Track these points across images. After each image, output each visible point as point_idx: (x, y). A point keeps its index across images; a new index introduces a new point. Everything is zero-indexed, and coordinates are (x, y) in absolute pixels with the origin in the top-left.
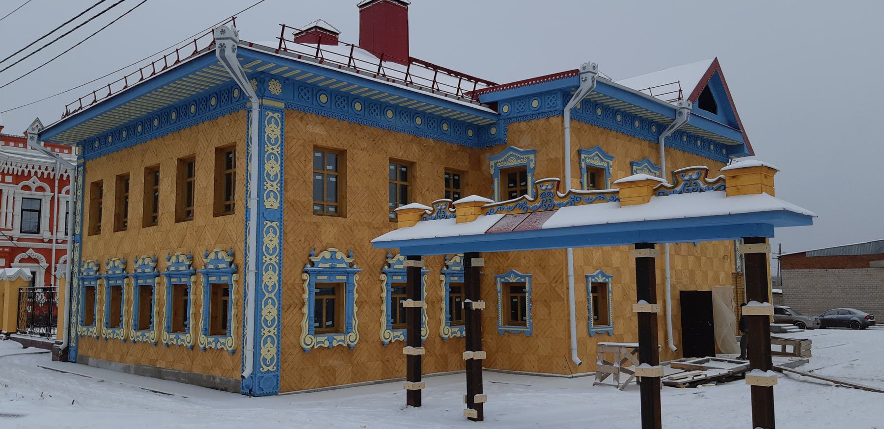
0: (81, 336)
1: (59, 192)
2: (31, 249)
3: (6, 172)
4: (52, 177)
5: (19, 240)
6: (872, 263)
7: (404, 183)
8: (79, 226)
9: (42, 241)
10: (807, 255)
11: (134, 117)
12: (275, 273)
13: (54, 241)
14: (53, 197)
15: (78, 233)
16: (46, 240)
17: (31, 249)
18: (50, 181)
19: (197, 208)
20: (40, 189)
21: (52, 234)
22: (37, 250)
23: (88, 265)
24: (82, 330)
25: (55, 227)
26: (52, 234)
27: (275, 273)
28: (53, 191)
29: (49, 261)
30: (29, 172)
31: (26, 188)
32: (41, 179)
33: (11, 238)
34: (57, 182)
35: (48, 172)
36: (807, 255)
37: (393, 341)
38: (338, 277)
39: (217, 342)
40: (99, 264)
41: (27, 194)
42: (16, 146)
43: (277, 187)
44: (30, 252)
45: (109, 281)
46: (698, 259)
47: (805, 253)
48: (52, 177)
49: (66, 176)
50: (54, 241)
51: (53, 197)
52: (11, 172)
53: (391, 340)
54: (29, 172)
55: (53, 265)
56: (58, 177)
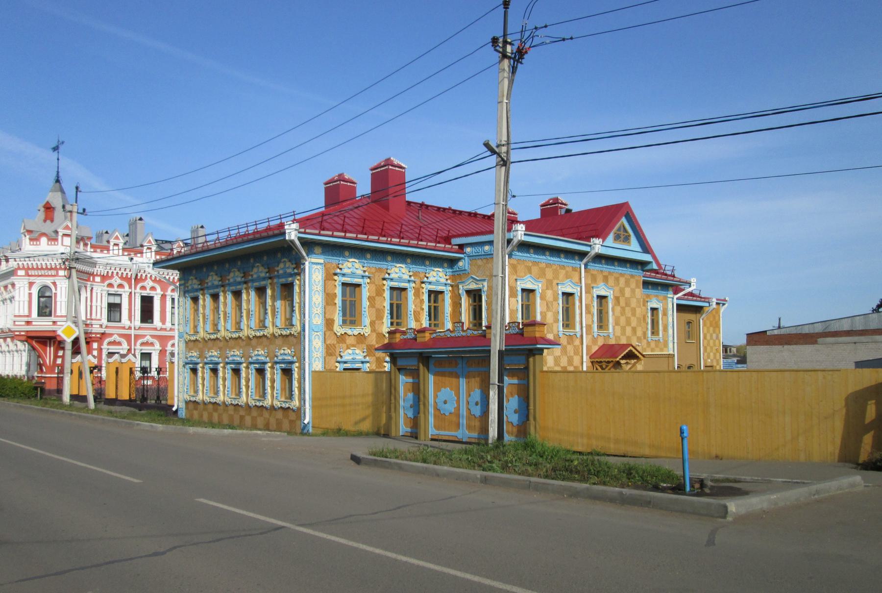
1: (135, 288)
2: (115, 335)
3: (95, 273)
4: (129, 277)
5: (107, 327)
6: (820, 340)
9: (124, 328)
10: (768, 333)
11: (482, 230)
12: (320, 362)
13: (133, 328)
14: (131, 293)
16: (127, 328)
17: (115, 335)
18: (128, 280)
20: (153, 288)
21: (131, 323)
22: (153, 337)
25: (133, 317)
26: (131, 323)
27: (320, 362)
28: (130, 287)
29: (129, 344)
30: (113, 272)
31: (110, 285)
32: (122, 278)
33: (101, 326)
34: (133, 281)
35: (126, 272)
36: (768, 333)
38: (357, 365)
41: (112, 290)
42: (102, 251)
44: (116, 338)
46: (715, 345)
47: (766, 332)
48: (129, 277)
49: (111, 273)
50: (133, 328)
51: (131, 293)
52: (99, 274)
54: (113, 272)
55: (133, 348)
56: (134, 276)
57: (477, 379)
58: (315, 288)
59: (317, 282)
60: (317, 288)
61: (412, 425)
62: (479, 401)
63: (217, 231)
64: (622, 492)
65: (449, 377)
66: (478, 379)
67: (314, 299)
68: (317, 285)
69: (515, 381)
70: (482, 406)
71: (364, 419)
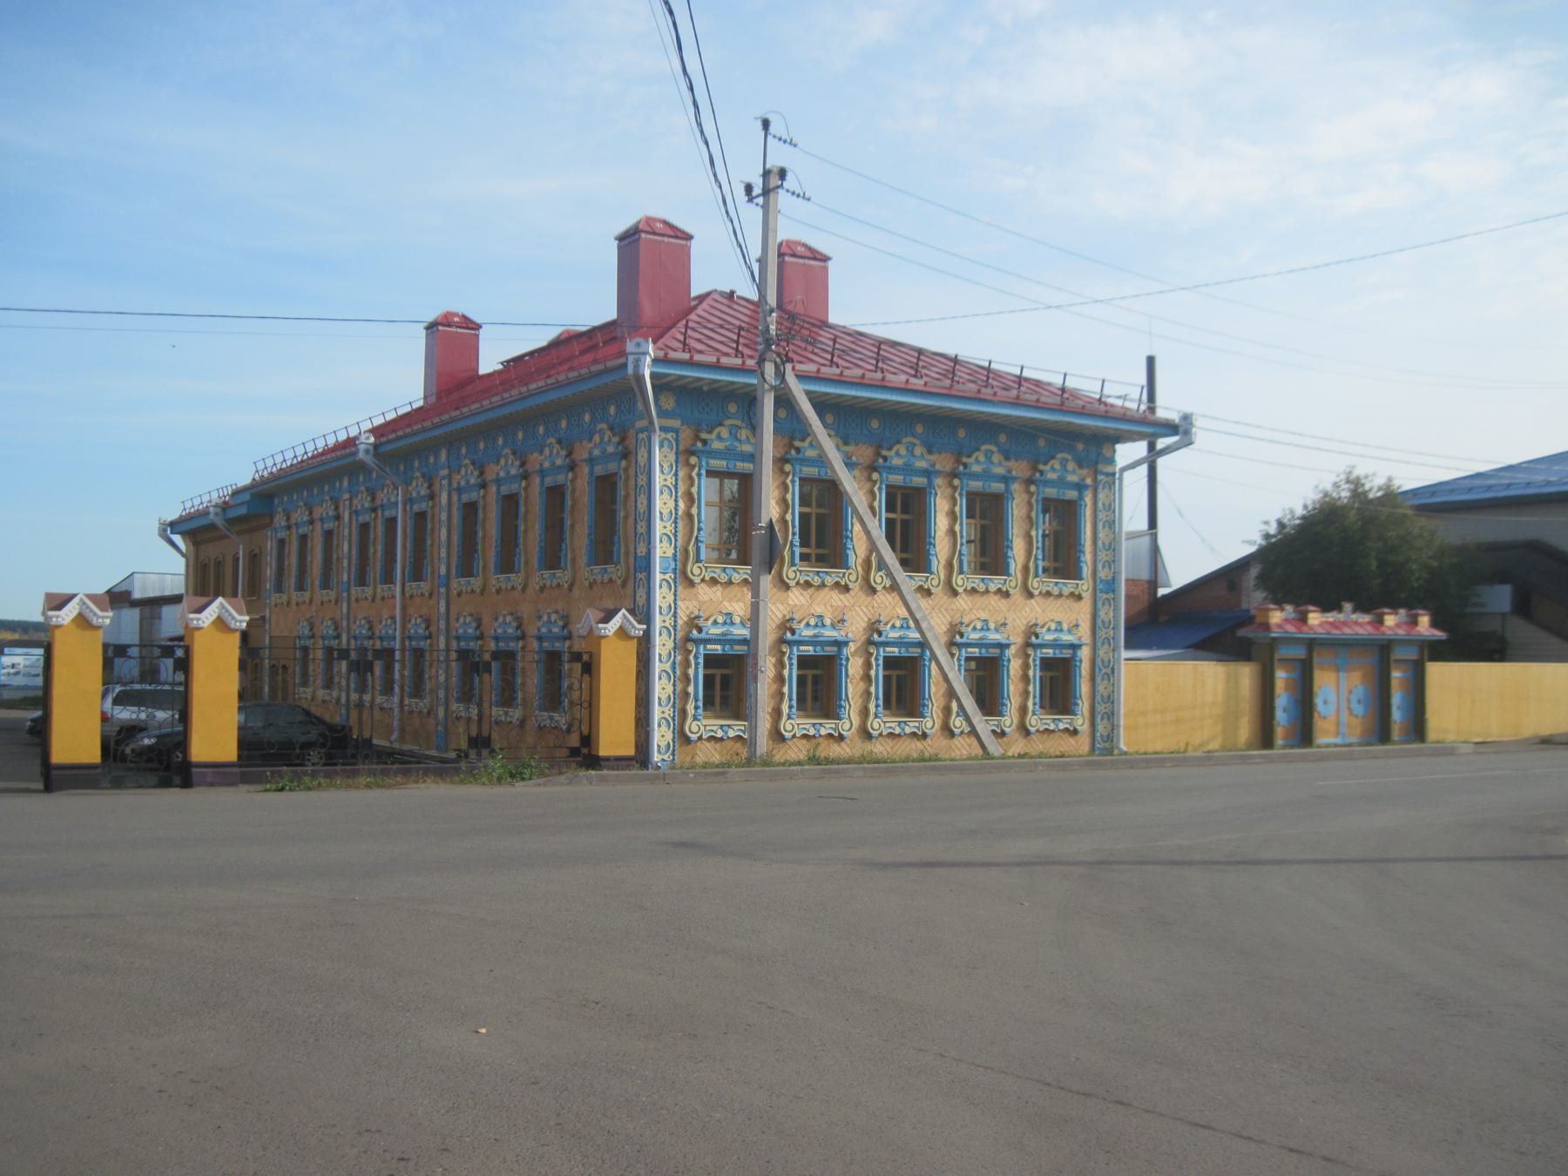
0: (497, 723)
7: (906, 517)
8: (644, 541)
15: (644, 554)
19: (521, 560)
23: (465, 620)
24: (497, 712)
37: (704, 737)
39: (506, 714)
40: (567, 616)
43: (671, 528)
45: (498, 642)
53: (701, 735)
58: (1102, 708)
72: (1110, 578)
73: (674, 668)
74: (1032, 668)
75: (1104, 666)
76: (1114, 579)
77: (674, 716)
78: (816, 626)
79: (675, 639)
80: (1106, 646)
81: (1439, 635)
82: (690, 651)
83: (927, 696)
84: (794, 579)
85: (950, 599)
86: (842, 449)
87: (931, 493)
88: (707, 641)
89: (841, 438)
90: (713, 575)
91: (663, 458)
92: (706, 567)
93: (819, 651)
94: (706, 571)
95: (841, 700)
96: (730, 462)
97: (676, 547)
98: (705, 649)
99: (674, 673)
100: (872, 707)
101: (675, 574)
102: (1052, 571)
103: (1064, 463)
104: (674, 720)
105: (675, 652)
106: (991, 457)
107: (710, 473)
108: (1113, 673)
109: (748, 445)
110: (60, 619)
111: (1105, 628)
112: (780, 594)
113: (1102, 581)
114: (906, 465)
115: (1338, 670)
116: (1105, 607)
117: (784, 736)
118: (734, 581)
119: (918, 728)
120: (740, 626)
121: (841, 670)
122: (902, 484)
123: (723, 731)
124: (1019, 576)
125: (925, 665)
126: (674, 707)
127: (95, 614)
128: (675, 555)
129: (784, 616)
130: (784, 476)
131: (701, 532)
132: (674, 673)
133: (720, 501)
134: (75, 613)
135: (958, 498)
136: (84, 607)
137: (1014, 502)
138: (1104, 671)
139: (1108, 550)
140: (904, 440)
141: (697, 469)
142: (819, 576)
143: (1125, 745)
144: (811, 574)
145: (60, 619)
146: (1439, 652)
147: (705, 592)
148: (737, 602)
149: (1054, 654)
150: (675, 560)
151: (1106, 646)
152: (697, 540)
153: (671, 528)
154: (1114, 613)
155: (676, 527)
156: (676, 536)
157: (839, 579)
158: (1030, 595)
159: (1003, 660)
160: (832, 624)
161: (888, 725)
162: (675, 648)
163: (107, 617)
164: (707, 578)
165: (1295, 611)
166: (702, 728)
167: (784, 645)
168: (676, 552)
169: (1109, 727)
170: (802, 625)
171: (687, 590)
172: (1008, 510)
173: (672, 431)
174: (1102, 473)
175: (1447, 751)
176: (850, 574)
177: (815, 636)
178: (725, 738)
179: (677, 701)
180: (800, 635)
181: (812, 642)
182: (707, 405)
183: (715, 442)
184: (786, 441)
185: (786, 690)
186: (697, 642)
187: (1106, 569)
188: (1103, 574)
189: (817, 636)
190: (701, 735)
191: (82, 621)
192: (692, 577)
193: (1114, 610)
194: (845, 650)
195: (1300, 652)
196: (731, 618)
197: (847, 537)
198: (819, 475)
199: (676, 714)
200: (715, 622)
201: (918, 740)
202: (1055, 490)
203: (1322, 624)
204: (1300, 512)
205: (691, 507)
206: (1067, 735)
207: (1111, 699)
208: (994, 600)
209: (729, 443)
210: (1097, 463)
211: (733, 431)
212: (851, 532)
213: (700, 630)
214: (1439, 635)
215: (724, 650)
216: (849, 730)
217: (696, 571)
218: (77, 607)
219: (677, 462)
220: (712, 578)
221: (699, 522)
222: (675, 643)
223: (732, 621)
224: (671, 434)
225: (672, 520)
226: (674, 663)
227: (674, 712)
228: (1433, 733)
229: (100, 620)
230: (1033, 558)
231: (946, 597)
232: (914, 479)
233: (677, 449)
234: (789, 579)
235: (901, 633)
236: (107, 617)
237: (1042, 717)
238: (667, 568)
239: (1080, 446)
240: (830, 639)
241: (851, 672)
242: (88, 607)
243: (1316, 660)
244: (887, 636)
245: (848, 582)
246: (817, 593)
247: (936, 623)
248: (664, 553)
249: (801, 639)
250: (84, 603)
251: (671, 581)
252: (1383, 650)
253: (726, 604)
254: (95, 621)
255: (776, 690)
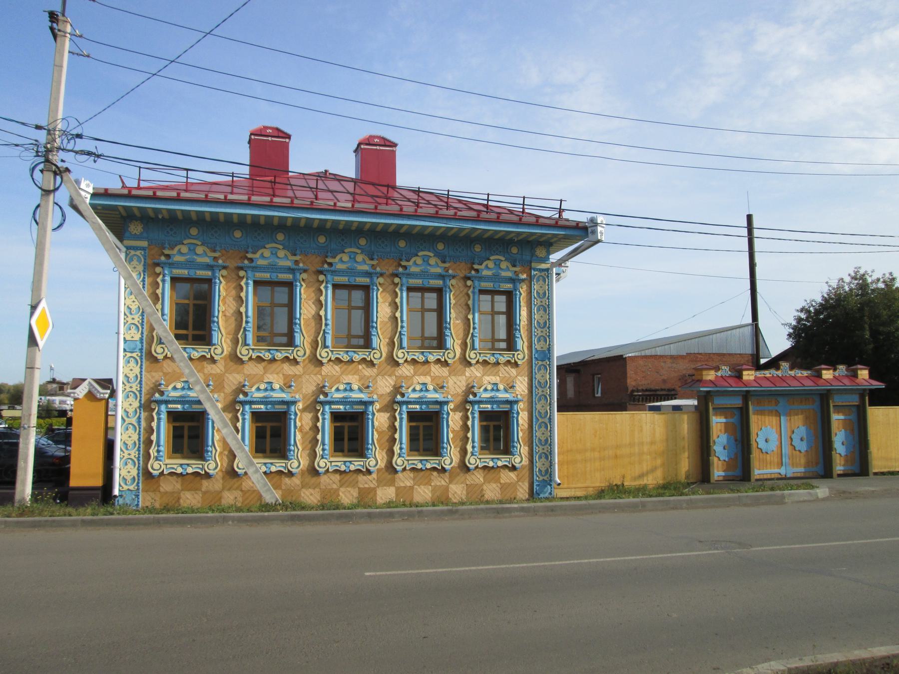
43: (138, 320)
57: (800, 416)
58: (540, 449)
59: (543, 440)
60: (543, 449)
61: (725, 468)
62: (805, 437)
63: (233, 173)
64: (783, 494)
65: (769, 415)
66: (801, 417)
67: (538, 376)
68: (543, 445)
69: (842, 417)
70: (808, 442)
71: (653, 470)
72: (545, 349)
73: (139, 422)
74: (241, 420)
75: (541, 417)
76: (549, 350)
77: (139, 457)
78: (421, 390)
79: (140, 400)
80: (543, 401)
81: (877, 385)
82: (396, 410)
83: (445, 441)
84: (163, 353)
85: (393, 369)
86: (290, 258)
87: (373, 289)
88: (480, 402)
89: (511, 262)
90: (338, 356)
91: (540, 288)
92: (480, 353)
93: (495, 408)
94: (480, 356)
95: (443, 443)
96: (191, 270)
97: (142, 333)
98: (407, 408)
99: (139, 425)
100: (469, 447)
101: (141, 352)
102: (190, 338)
103: (497, 264)
104: (139, 460)
105: (140, 410)
106: (499, 265)
107: (483, 292)
108: (550, 422)
109: (438, 268)
110: (76, 395)
111: (542, 387)
112: (235, 366)
113: (537, 351)
114: (494, 275)
115: (778, 414)
116: (541, 372)
117: (396, 469)
118: (500, 362)
119: (363, 467)
120: (279, 391)
121: (513, 420)
122: (348, 283)
123: (422, 464)
124: (526, 351)
125: (513, 417)
126: (139, 450)
127: (98, 392)
128: (141, 339)
129: (319, 385)
130: (467, 288)
131: (476, 330)
132: (139, 425)
133: (492, 311)
134: (86, 391)
135: (471, 295)
136: (91, 387)
137: (452, 293)
138: (541, 420)
139: (543, 328)
140: (346, 251)
141: (472, 288)
142: (494, 356)
143: (559, 478)
144: (263, 352)
145: (76, 395)
146: (879, 398)
147: (253, 369)
148: (271, 374)
149: (492, 408)
150: (142, 343)
151: (543, 401)
152: (473, 336)
153: (138, 320)
154: (550, 376)
155: (143, 319)
156: (142, 325)
157: (510, 359)
158: (470, 364)
159: (513, 413)
160: (504, 388)
161: (410, 462)
162: (140, 407)
163: (106, 393)
164: (481, 361)
165: (847, 370)
166: (328, 463)
167: (468, 404)
168: (142, 336)
169: (547, 464)
170: (410, 390)
171: (153, 364)
172: (373, 298)
173: (140, 249)
174: (535, 270)
175: (713, 484)
176: (449, 353)
177: (420, 398)
178: (495, 467)
179: (142, 445)
180: (252, 397)
181: (491, 401)
182: (383, 242)
183: (413, 267)
184: (469, 265)
185: (470, 435)
186: (400, 404)
187: (542, 342)
188: (537, 346)
189: (422, 398)
190: (405, 467)
191: (91, 395)
192: (398, 360)
193: (550, 373)
194: (516, 406)
195: (738, 402)
196: (426, 387)
197: (516, 329)
198: (271, 278)
199: (141, 456)
200: (486, 390)
201: (364, 475)
202: (347, 278)
203: (756, 380)
204: (819, 300)
205: (396, 312)
206: (507, 470)
207: (548, 442)
208: (436, 370)
209: (423, 267)
210: (531, 262)
211: (352, 257)
212: (519, 326)
213: (475, 395)
214: (877, 385)
215: (266, 408)
216: (450, 464)
217: (400, 355)
218: (87, 387)
219: (144, 271)
220: (413, 359)
221: (474, 323)
222: (140, 403)
223: (426, 389)
224: (140, 251)
225: (140, 313)
226: (139, 418)
227: (139, 454)
228: (878, 463)
229: (102, 395)
230: (470, 335)
231: (389, 367)
232: (357, 279)
233: (145, 262)
234: (471, 359)
235: (492, 394)
236: (106, 393)
237: (480, 457)
238: (135, 349)
239: (514, 250)
240: (278, 399)
241: (521, 421)
242: (94, 387)
243: (751, 408)
244: (480, 397)
245: (517, 360)
246: (270, 365)
247: (456, 385)
248: (132, 337)
249: (408, 400)
250: (92, 385)
251: (138, 358)
252: (824, 398)
253: (479, 375)
254: (98, 396)
255: (390, 436)
